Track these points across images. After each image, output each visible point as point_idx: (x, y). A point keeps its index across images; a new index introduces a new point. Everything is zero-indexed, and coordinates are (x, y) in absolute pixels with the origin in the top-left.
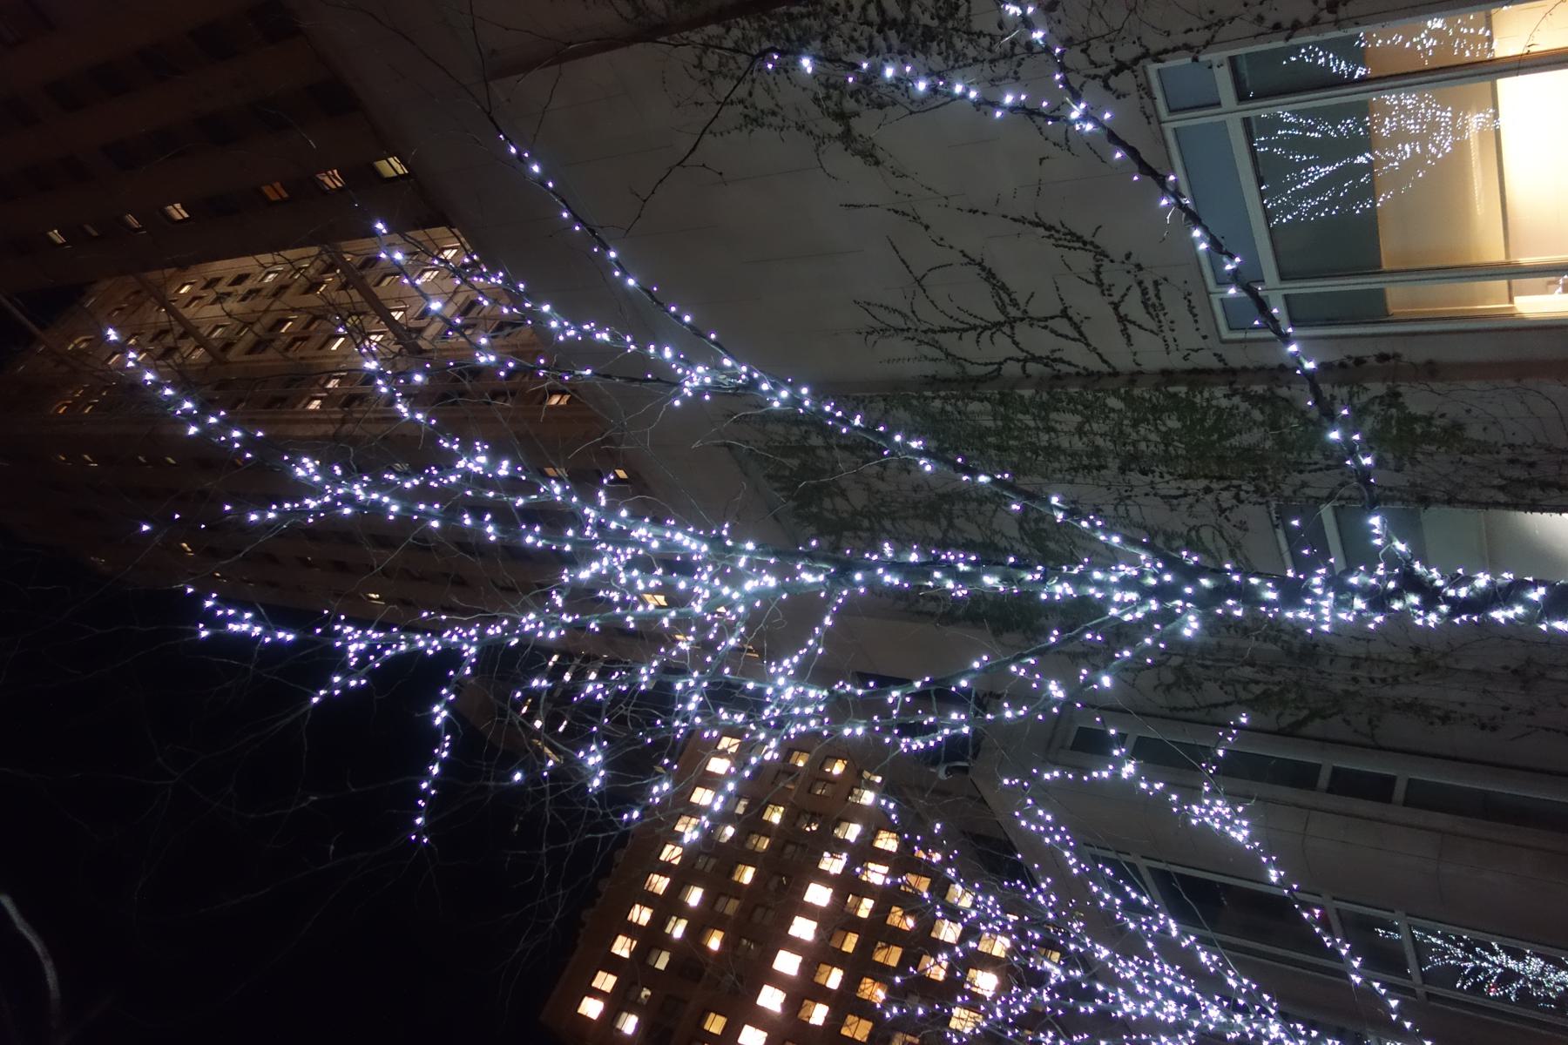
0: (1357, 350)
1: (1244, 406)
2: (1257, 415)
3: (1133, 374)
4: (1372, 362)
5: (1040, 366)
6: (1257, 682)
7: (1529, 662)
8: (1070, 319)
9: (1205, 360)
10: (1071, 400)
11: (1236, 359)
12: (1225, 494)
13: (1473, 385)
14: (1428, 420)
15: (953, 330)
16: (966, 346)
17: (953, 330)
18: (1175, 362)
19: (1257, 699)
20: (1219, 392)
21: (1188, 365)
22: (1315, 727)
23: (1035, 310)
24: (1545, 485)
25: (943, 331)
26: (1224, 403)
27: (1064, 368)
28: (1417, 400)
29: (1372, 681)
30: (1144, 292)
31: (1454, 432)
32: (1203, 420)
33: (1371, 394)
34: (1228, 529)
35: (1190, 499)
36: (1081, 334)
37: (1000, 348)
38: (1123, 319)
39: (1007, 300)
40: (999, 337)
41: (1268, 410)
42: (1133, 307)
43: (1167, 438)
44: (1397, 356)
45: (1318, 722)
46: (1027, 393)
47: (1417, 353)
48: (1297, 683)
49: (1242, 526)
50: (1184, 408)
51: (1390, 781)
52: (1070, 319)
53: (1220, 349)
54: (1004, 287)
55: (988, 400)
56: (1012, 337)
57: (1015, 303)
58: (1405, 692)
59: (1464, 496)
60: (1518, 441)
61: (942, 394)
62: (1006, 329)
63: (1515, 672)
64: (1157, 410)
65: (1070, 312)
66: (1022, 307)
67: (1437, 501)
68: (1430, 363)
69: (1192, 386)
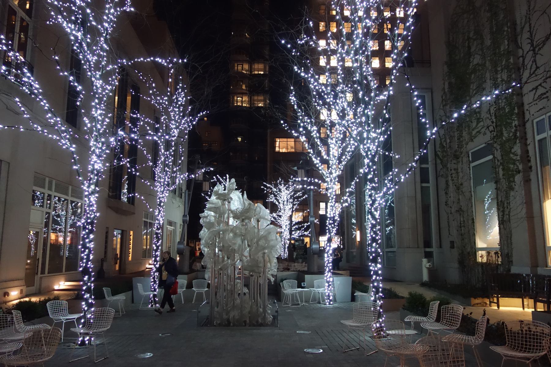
0: (533, 159)
1: (513, 130)
2: (511, 134)
3: (522, 94)
4: (530, 164)
5: (522, 62)
6: (446, 144)
7: (463, 211)
8: (536, 70)
9: (527, 116)
10: (511, 76)
11: (528, 125)
12: (492, 127)
13: (523, 192)
14: (514, 181)
15: (530, 28)
16: (526, 35)
17: (530, 28)
18: (526, 107)
19: (443, 145)
20: (516, 123)
21: (525, 111)
22: (439, 161)
23: (538, 57)
24: (503, 211)
25: (530, 25)
26: (513, 124)
27: (522, 71)
28: (518, 178)
29: (452, 174)
30: (545, 94)
31: (511, 188)
32: (509, 119)
33: (519, 166)
34: (483, 130)
35: (490, 117)
36: (532, 74)
37: (527, 47)
38: (536, 88)
39: (540, 46)
40: (530, 45)
41: (513, 137)
42: (541, 91)
43: (504, 108)
44: (531, 171)
45: (440, 161)
46: (511, 60)
47: (533, 176)
48: (448, 155)
49: (485, 134)
50: (511, 113)
51: (428, 182)
52: (536, 70)
53: (530, 121)
54: (544, 44)
55: (508, 47)
56: (530, 51)
57: (540, 49)
58: (450, 183)
59: (499, 192)
60: (511, 204)
61: (509, 30)
62: (532, 48)
63: (460, 208)
64: (510, 104)
65: (538, 69)
66: (539, 52)
67: (497, 185)
68: (530, 180)
69: (518, 114)
